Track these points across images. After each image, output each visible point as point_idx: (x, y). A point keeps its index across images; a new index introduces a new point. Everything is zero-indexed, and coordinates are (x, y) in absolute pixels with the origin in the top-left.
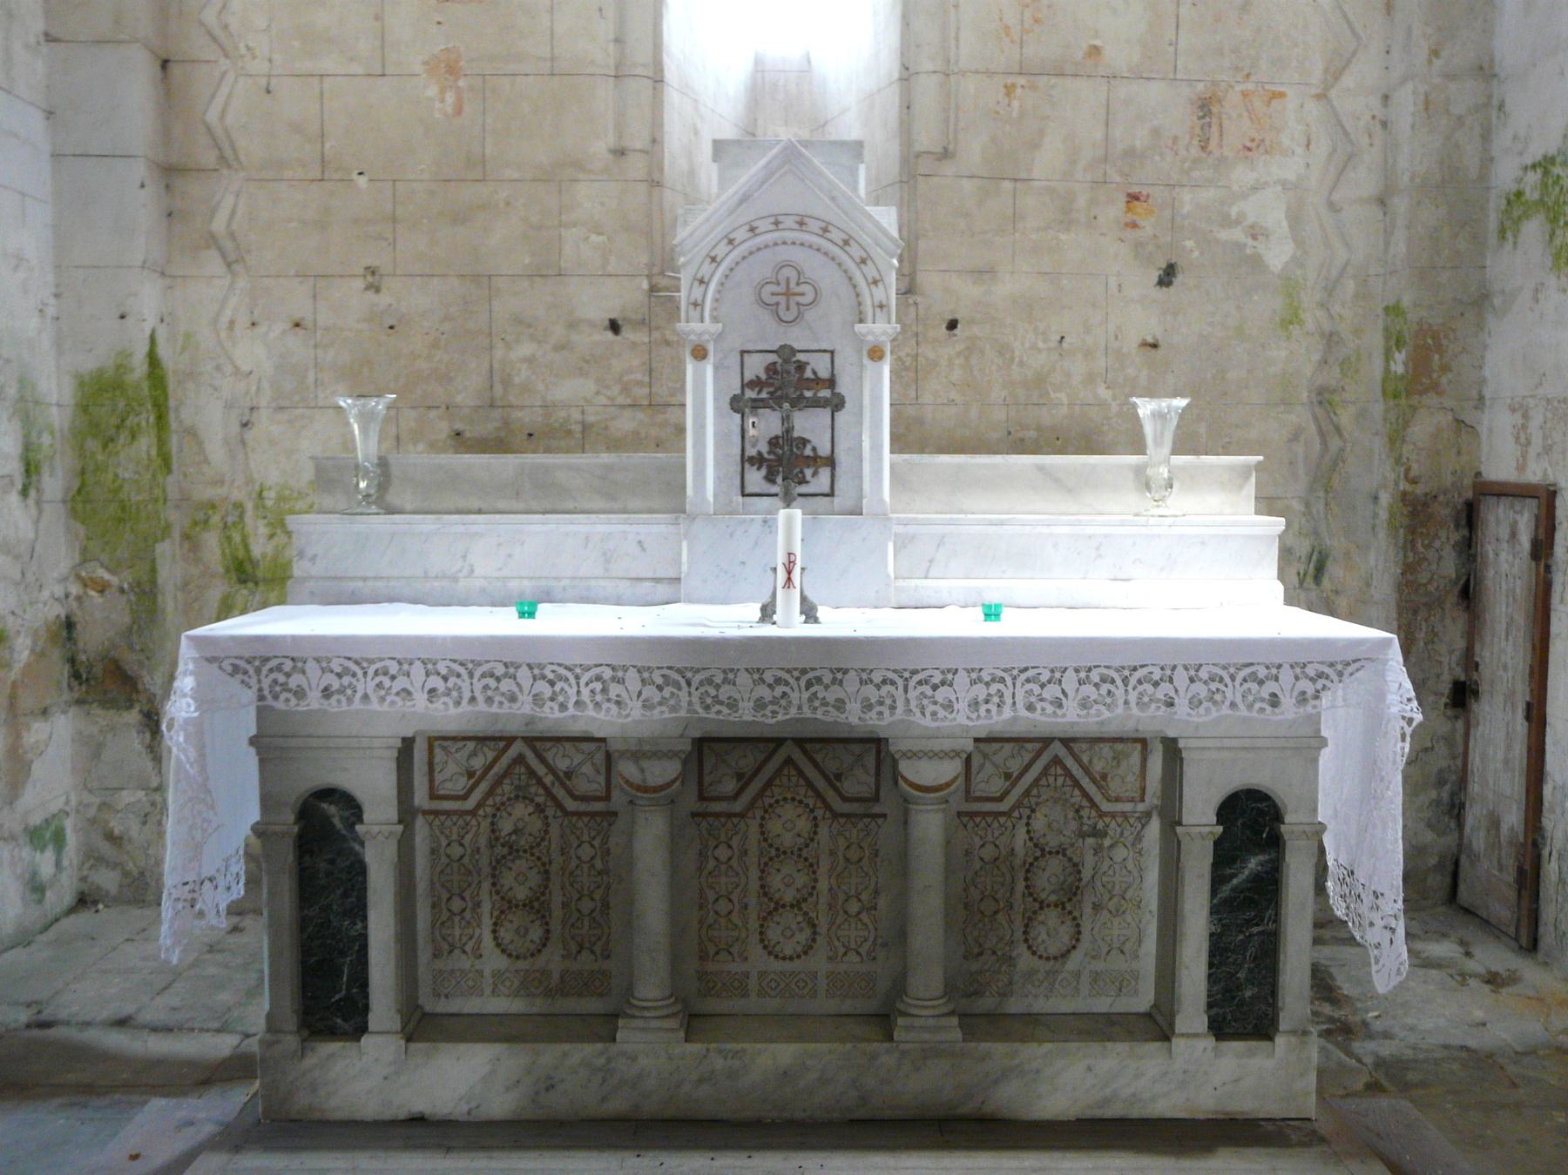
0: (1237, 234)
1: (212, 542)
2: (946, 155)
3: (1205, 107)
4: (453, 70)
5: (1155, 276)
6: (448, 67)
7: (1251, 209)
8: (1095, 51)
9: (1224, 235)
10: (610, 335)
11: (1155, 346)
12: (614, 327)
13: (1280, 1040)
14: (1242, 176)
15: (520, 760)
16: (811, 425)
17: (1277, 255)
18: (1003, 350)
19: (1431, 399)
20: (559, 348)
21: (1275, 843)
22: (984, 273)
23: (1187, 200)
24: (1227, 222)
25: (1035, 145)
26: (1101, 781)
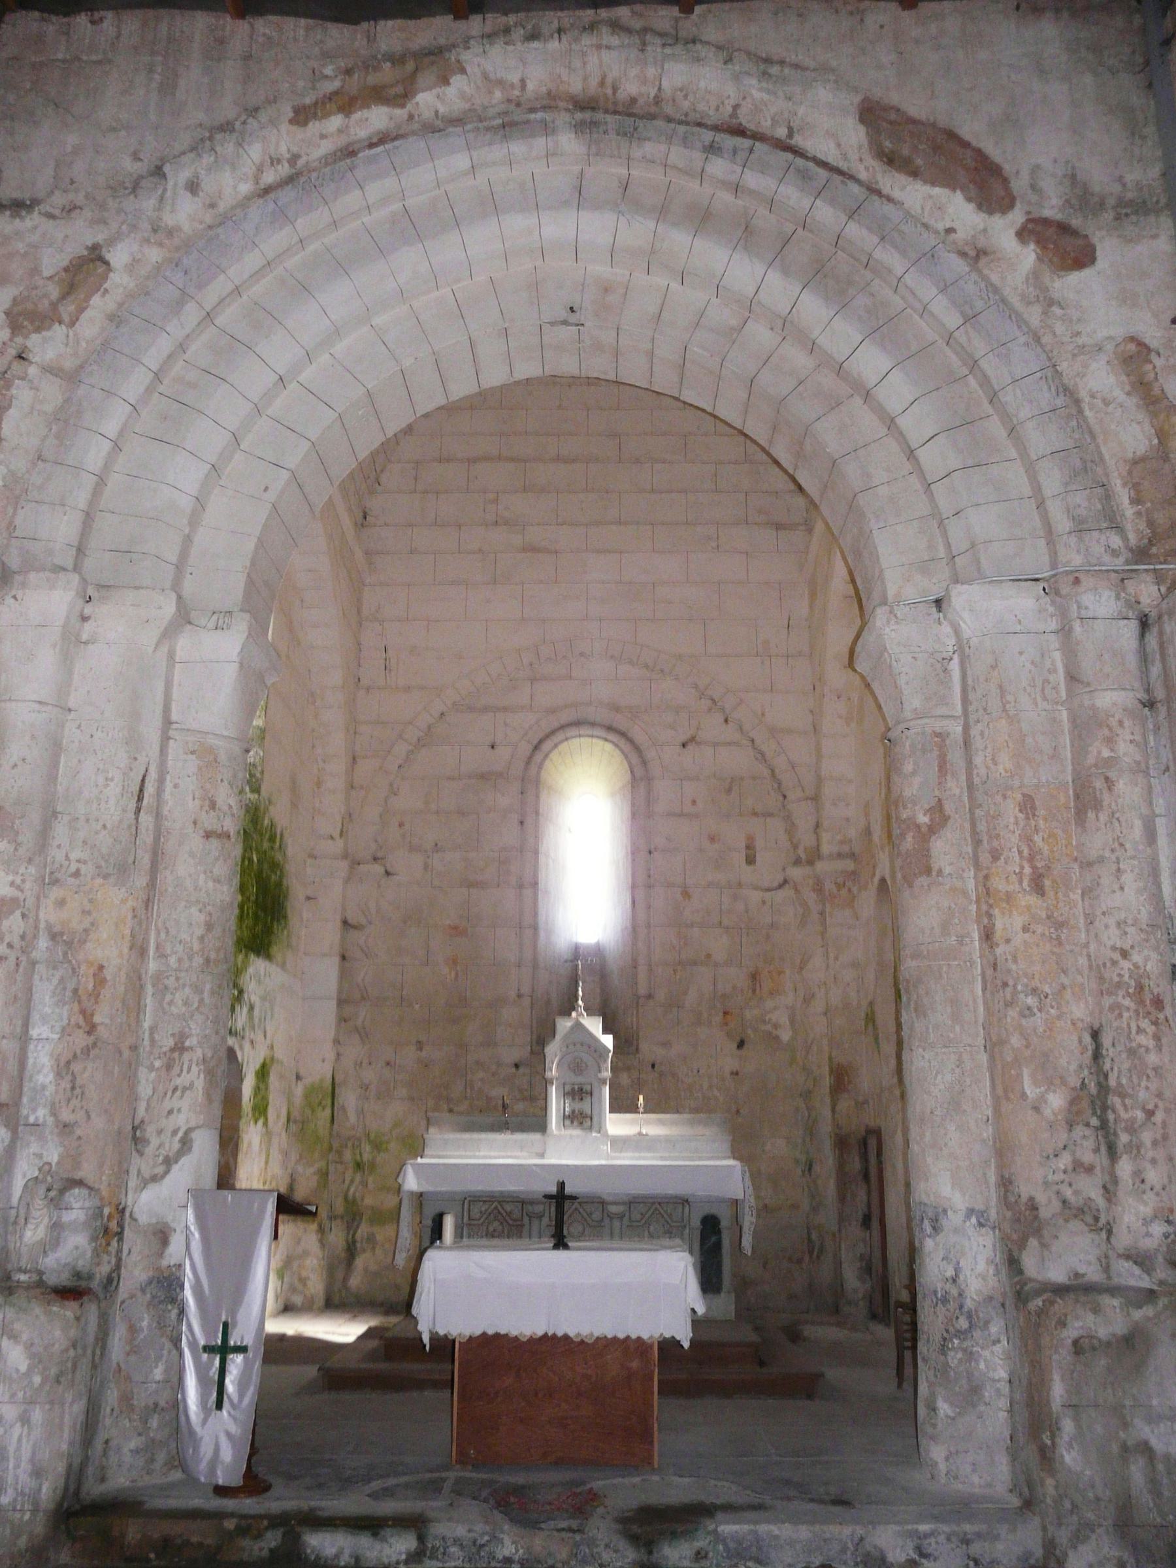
0: (768, 1027)
1: (348, 1155)
2: (650, 996)
3: (754, 976)
4: (455, 962)
5: (735, 1045)
6: (454, 962)
7: (774, 1017)
8: (709, 956)
9: (763, 1027)
10: (514, 1070)
11: (737, 1074)
12: (517, 1066)
13: (723, 1294)
14: (769, 1004)
15: (496, 1208)
16: (585, 1106)
17: (785, 1036)
18: (674, 1075)
19: (846, 1095)
20: (493, 1075)
21: (719, 1232)
22: (666, 1044)
23: (748, 1014)
24: (764, 1022)
25: (685, 993)
26: (670, 1215)
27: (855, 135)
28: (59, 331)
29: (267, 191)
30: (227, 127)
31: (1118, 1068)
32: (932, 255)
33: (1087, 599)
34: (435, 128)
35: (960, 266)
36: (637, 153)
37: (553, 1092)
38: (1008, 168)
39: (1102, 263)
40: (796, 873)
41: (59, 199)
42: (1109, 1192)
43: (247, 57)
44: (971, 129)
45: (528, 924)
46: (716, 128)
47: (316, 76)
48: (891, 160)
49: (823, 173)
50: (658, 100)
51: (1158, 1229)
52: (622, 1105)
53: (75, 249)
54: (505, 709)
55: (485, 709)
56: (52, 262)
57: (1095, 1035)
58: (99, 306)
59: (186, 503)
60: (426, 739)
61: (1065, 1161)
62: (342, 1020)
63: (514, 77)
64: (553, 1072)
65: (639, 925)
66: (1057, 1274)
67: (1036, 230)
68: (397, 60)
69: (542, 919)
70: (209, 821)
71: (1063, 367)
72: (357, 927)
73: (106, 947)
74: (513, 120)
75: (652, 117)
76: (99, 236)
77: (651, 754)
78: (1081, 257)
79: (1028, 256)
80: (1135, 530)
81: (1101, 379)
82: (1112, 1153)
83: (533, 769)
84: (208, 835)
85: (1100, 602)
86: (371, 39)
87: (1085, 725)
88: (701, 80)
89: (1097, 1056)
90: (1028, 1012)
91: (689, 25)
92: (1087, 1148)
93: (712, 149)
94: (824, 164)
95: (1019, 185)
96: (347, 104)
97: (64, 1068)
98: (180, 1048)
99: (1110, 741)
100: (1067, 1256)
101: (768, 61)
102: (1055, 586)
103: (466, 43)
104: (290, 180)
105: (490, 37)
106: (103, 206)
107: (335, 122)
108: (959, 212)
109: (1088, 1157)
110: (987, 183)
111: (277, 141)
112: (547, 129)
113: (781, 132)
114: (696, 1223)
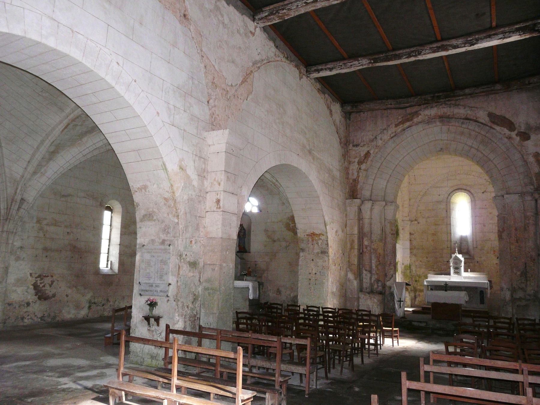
1: (414, 279)
6: (433, 240)
27: (487, 119)
29: (392, 138)
30: (385, 129)
32: (501, 139)
33: (526, 197)
35: (506, 140)
36: (450, 124)
37: (452, 268)
38: (515, 123)
39: (532, 139)
41: (362, 144)
42: (526, 286)
43: (387, 116)
45: (449, 232)
46: (463, 119)
47: (398, 119)
48: (494, 123)
49: (482, 125)
50: (453, 115)
51: (532, 291)
52: (466, 271)
54: (439, 187)
55: (437, 187)
56: (363, 154)
57: (526, 264)
58: (370, 159)
59: (384, 187)
60: (425, 194)
61: (520, 281)
62: (411, 253)
63: (429, 114)
64: (451, 264)
65: (474, 232)
67: (519, 134)
68: (410, 114)
69: (452, 231)
70: (392, 232)
71: (525, 157)
72: (413, 234)
73: (380, 251)
74: (430, 121)
75: (452, 118)
77: (475, 195)
79: (518, 138)
82: (527, 281)
83: (449, 200)
84: (392, 234)
85: (528, 198)
86: (406, 111)
87: (526, 217)
88: (461, 111)
89: (526, 267)
90: (515, 260)
91: (457, 103)
93: (463, 123)
94: (482, 123)
95: (517, 126)
96: (402, 123)
97: (376, 267)
98: (391, 263)
99: (529, 220)
100: (520, 294)
101: (472, 107)
102: (522, 194)
103: (421, 110)
104: (395, 135)
106: (368, 144)
108: (506, 131)
110: (511, 126)
111: (392, 130)
112: (435, 122)
113: (475, 118)
114: (479, 292)
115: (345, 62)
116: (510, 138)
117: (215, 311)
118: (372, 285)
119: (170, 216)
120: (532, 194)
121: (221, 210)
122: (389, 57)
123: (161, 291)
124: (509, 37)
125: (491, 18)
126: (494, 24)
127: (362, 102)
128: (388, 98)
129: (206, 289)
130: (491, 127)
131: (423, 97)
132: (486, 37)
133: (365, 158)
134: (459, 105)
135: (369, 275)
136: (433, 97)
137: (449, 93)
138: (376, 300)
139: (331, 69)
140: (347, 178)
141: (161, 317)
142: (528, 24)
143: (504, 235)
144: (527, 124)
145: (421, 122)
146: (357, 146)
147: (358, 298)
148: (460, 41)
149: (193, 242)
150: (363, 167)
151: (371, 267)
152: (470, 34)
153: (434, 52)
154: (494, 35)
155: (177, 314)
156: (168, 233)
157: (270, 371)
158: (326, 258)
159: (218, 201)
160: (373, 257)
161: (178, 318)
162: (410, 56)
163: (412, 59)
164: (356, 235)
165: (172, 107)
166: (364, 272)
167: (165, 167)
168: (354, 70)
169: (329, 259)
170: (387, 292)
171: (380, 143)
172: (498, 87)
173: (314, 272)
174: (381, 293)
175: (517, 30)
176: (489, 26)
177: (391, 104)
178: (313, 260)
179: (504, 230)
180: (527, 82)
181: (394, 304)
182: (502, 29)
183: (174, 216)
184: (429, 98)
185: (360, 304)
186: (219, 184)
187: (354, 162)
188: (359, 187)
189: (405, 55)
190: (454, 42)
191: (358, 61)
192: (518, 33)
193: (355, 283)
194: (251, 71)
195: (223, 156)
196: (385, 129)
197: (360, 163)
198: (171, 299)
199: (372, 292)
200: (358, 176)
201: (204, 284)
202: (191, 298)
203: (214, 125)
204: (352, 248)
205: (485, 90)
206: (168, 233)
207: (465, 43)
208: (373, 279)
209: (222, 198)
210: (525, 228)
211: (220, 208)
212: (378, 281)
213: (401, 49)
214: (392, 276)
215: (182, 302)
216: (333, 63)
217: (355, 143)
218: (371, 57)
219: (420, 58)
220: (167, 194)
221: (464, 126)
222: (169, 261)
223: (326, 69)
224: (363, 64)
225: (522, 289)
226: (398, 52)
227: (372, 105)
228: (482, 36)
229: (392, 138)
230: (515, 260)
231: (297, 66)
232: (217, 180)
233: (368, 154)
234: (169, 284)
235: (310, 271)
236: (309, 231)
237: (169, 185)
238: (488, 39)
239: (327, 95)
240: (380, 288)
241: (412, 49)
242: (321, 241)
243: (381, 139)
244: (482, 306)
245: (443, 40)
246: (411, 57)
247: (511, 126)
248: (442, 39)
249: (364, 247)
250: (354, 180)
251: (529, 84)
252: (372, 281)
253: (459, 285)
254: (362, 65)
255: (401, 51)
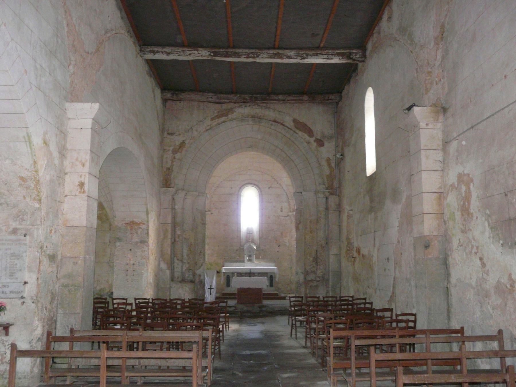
3: (282, 233)
16: (251, 258)
17: (288, 244)
27: (292, 124)
28: (179, 154)
29: (207, 130)
30: (201, 121)
31: (319, 255)
34: (232, 120)
35: (306, 144)
40: (290, 214)
41: (177, 133)
42: (317, 270)
44: (309, 124)
48: (297, 128)
49: (287, 129)
53: (181, 141)
54: (234, 181)
56: (178, 143)
58: (184, 149)
66: (309, 279)
76: (184, 139)
78: (322, 145)
79: (315, 144)
80: (327, 185)
81: (324, 163)
85: (321, 195)
86: (222, 106)
88: (270, 114)
90: (308, 248)
92: (314, 265)
93: (272, 125)
94: (288, 127)
95: (315, 133)
96: (218, 117)
97: (188, 255)
98: (200, 252)
100: (311, 277)
102: (316, 192)
104: (210, 129)
105: (239, 106)
107: (217, 119)
108: (306, 136)
109: (314, 266)
110: (310, 132)
113: (282, 122)
115: (184, 49)
116: (308, 143)
117: (78, 311)
118: (183, 274)
119: (28, 199)
120: (324, 192)
121: (86, 194)
122: (229, 53)
123: (12, 292)
124: (332, 59)
125: (322, 40)
126: (322, 45)
127: (183, 91)
128: (209, 91)
129: (65, 286)
130: (295, 132)
131: (243, 96)
132: (314, 55)
133: (180, 147)
134: (269, 108)
135: (181, 264)
136: (251, 97)
137: (265, 96)
138: (187, 289)
139: (168, 54)
140: (162, 167)
141: (12, 325)
142: (345, 51)
143: (301, 227)
144: (322, 132)
145: (234, 119)
146: (172, 134)
147: (170, 287)
148: (292, 53)
149: (53, 232)
150: (178, 156)
151: (182, 256)
152: (301, 49)
153: (271, 57)
154: (320, 54)
155: (36, 319)
156: (23, 220)
157: (162, 368)
158: (146, 248)
159: (82, 185)
160: (185, 247)
161: (37, 322)
162: (248, 57)
163: (251, 60)
164: (170, 225)
165: (38, 66)
166: (176, 261)
167: (29, 140)
168: (192, 59)
169: (149, 249)
170: (197, 281)
171: (195, 134)
172: (305, 97)
173: (132, 262)
174: (192, 282)
175: (338, 54)
176: (317, 45)
177: (212, 98)
178: (131, 250)
179: (300, 222)
180: (327, 98)
181: (204, 292)
182: (327, 51)
183: (34, 199)
184: (248, 98)
185: (172, 293)
186: (83, 165)
187: (169, 150)
188: (172, 176)
189: (244, 55)
190: (288, 52)
191: (198, 51)
192: (338, 58)
193: (168, 272)
194: (103, 40)
195: (88, 133)
196: (201, 121)
197: (175, 152)
198: (29, 301)
199: (183, 281)
200: (172, 165)
201: (62, 280)
202: (49, 298)
203: (74, 96)
204: (165, 237)
205: (295, 98)
206: (23, 220)
207: (297, 56)
208: (184, 268)
209: (86, 182)
210: (318, 221)
211: (84, 192)
212: (189, 269)
213: (239, 48)
214: (202, 264)
215: (42, 303)
216: (171, 48)
217: (170, 132)
218: (211, 50)
219: (258, 60)
220: (27, 173)
221: (272, 127)
222: (24, 255)
223: (162, 52)
224: (202, 54)
225: (314, 272)
226: (237, 51)
227: (193, 96)
228: (311, 53)
229: (207, 130)
230: (308, 248)
231: (134, 43)
232: (79, 160)
233: (183, 143)
234: (26, 283)
235: (128, 262)
236: (128, 220)
237: (32, 162)
238: (315, 57)
239: (152, 79)
240: (191, 276)
241: (251, 51)
242: (141, 230)
243: (197, 131)
244: (271, 289)
245: (279, 48)
246: (249, 57)
247: (310, 132)
248: (277, 46)
249: (177, 236)
250: (168, 169)
251: (328, 100)
252: (184, 270)
253: (266, 271)
254: (202, 56)
255: (241, 51)
